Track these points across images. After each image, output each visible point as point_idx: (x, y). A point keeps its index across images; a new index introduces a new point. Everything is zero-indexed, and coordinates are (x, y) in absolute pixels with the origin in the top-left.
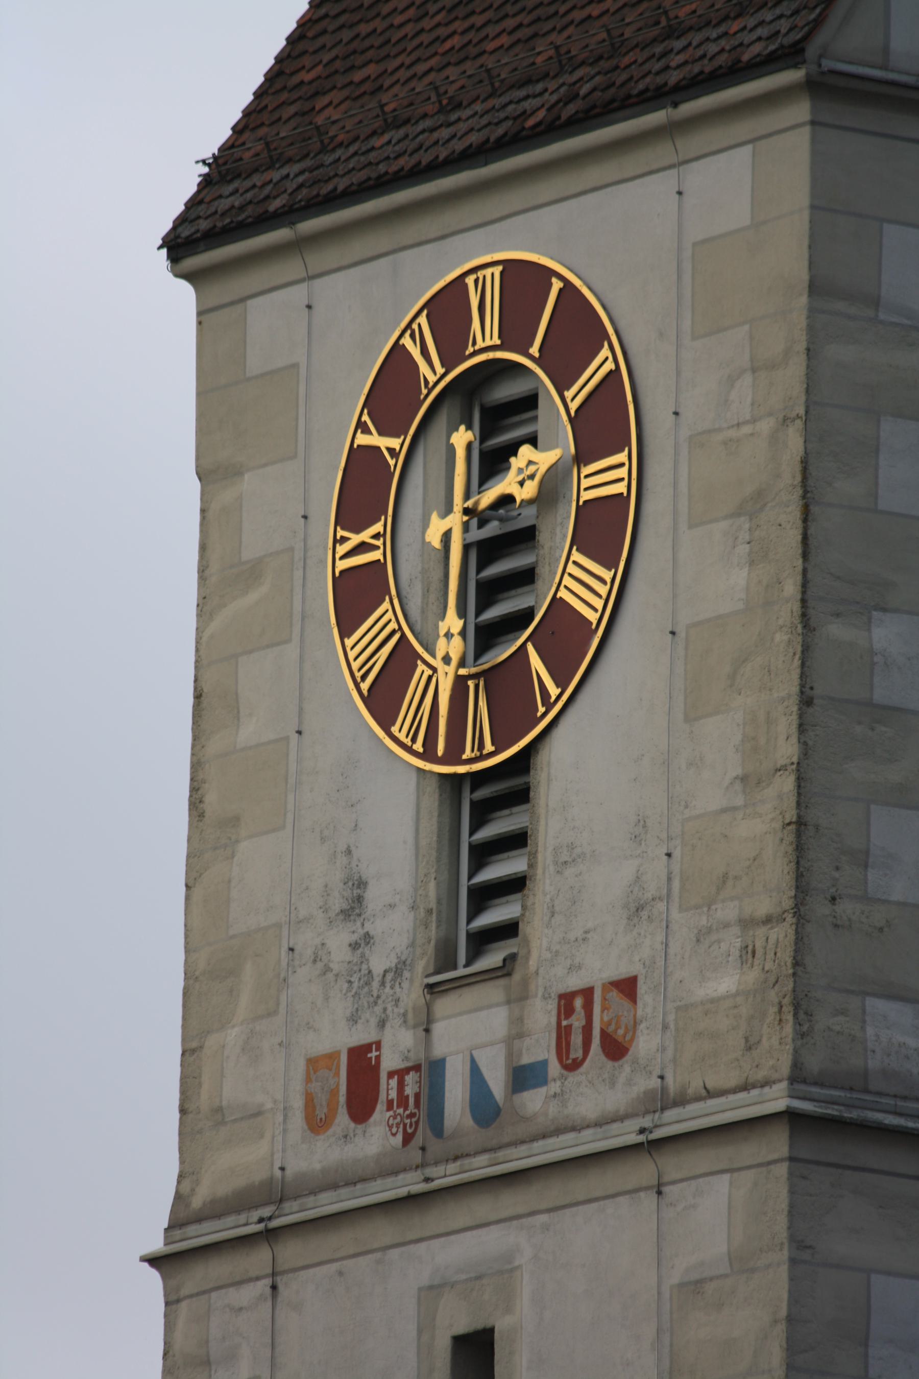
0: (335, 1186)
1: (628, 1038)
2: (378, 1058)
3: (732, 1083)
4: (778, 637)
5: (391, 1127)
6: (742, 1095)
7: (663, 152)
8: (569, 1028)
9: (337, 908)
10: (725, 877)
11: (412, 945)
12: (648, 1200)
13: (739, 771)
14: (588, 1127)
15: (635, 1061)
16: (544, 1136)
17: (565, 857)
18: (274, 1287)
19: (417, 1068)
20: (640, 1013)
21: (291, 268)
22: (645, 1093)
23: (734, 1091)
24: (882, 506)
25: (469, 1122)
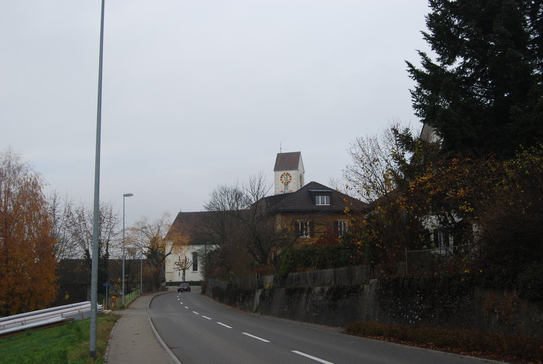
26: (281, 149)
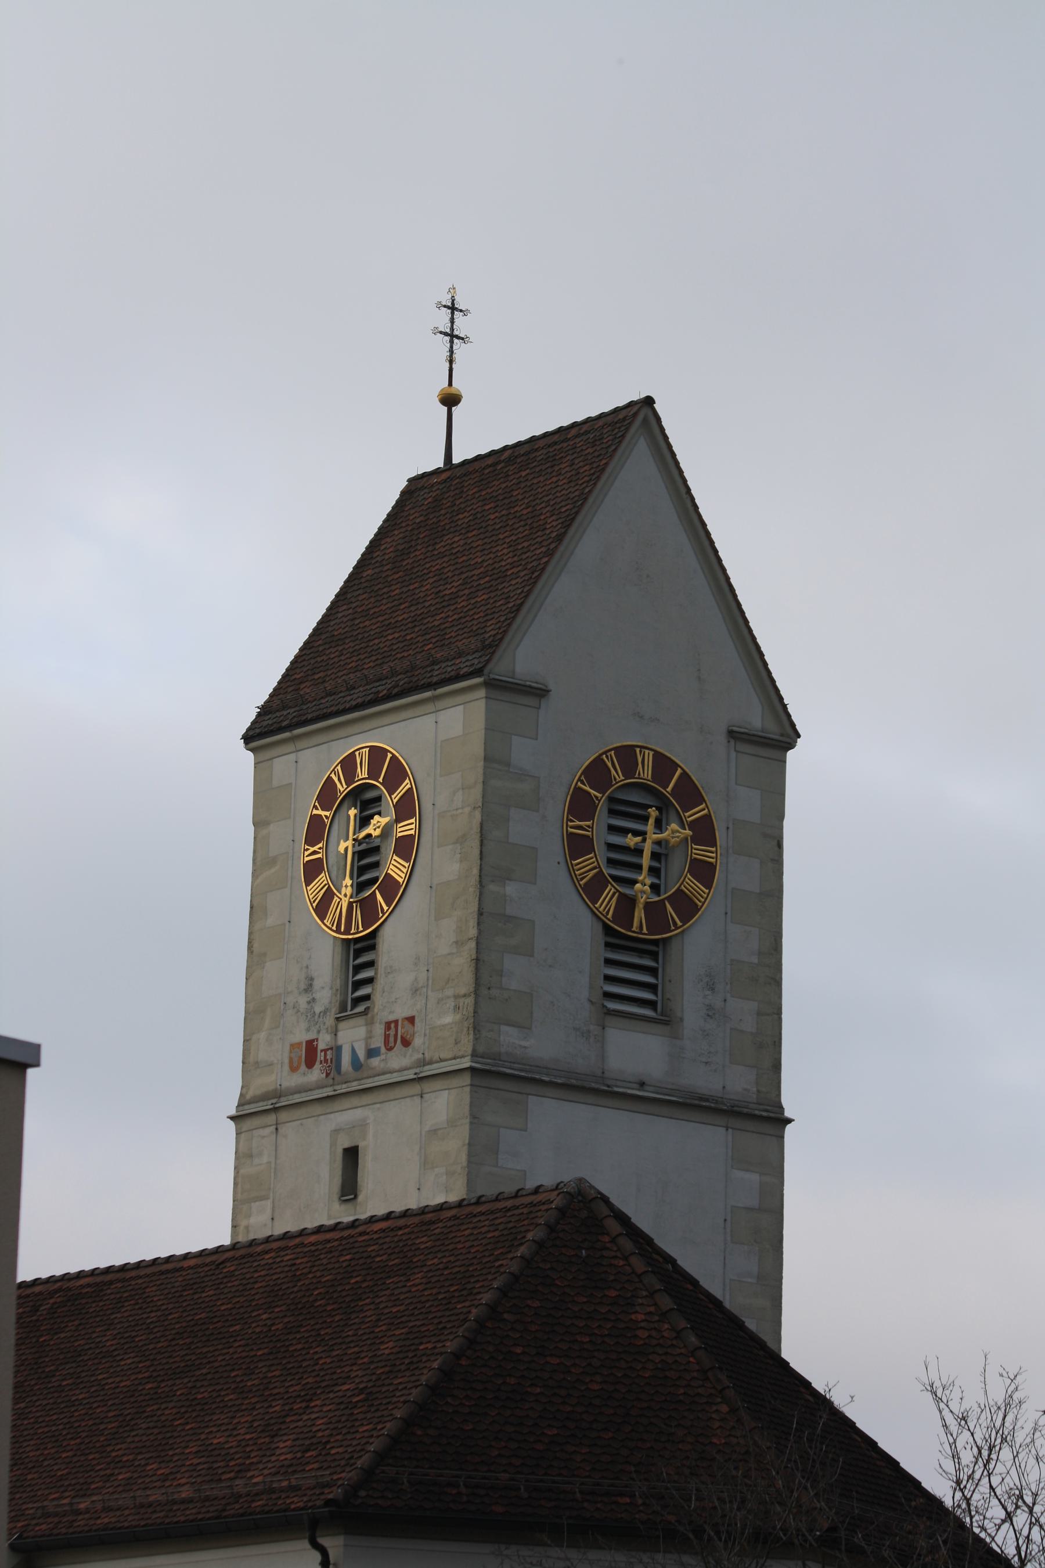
2: (317, 1045)
6: (454, 1061)
8: (389, 1034)
9: (302, 988)
12: (417, 1099)
13: (455, 940)
21: (290, 747)
25: (350, 1069)
26: (450, 400)
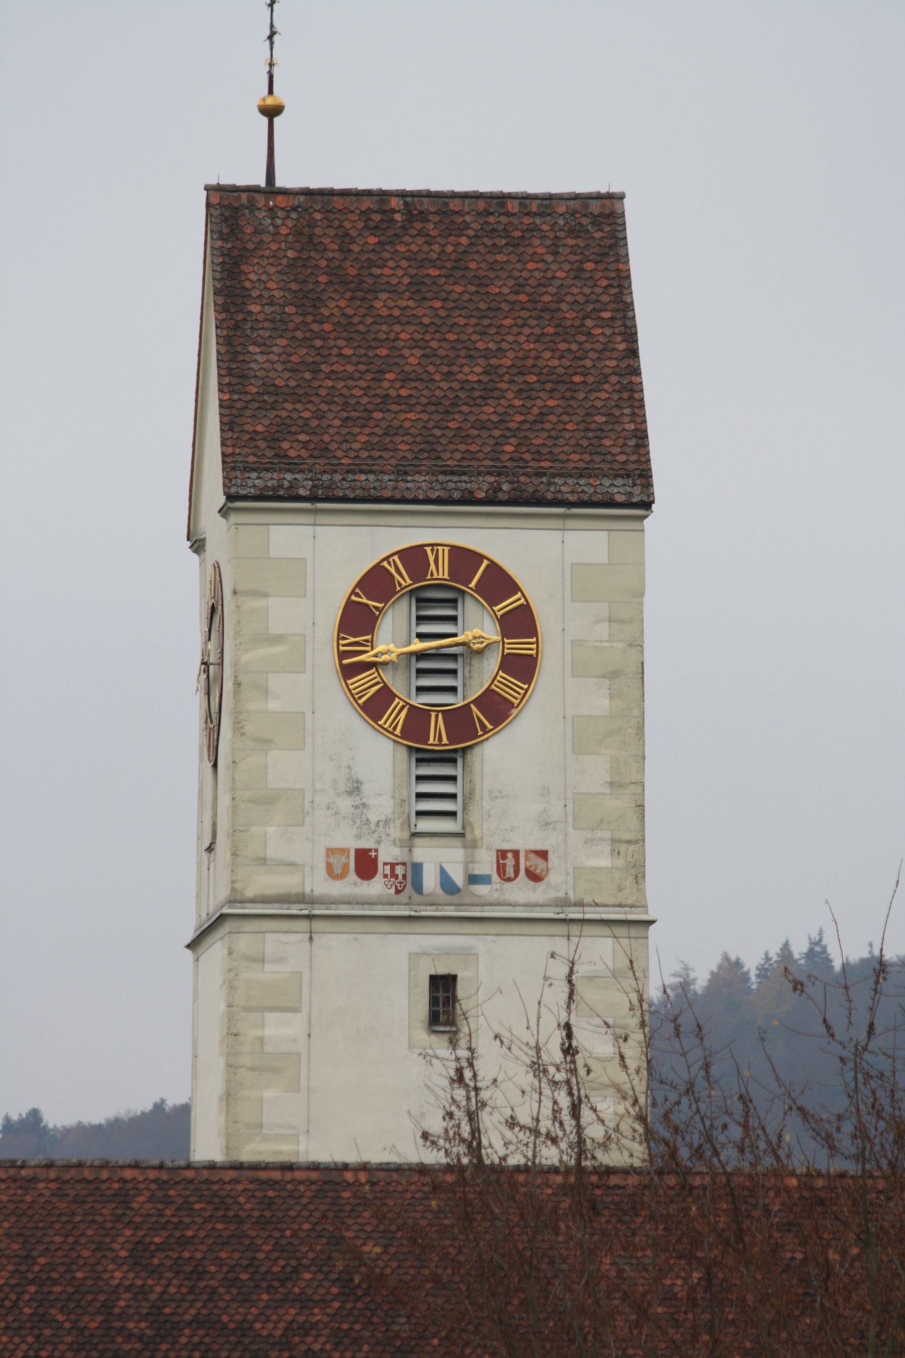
0: (349, 903)
1: (543, 874)
2: (376, 856)
3: (612, 901)
4: (629, 730)
5: (387, 885)
7: (558, 523)
8: (504, 865)
10: (602, 821)
11: (394, 812)
14: (519, 905)
15: (548, 884)
16: (491, 905)
17: (496, 794)
18: (311, 938)
19: (404, 864)
20: (550, 865)
22: (555, 898)
23: (613, 906)
24: (271, 556)
25: (439, 891)
